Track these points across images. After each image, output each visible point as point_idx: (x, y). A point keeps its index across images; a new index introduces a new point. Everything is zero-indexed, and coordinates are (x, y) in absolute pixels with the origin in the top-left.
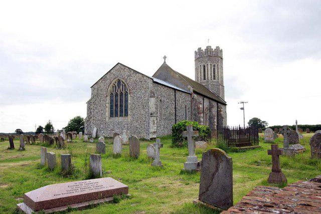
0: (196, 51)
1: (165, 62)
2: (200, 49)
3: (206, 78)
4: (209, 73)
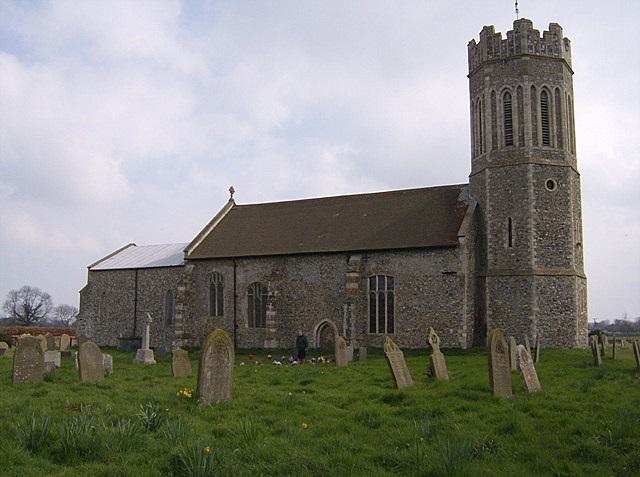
0: (472, 44)
2: (488, 32)
3: (516, 138)
4: (528, 111)
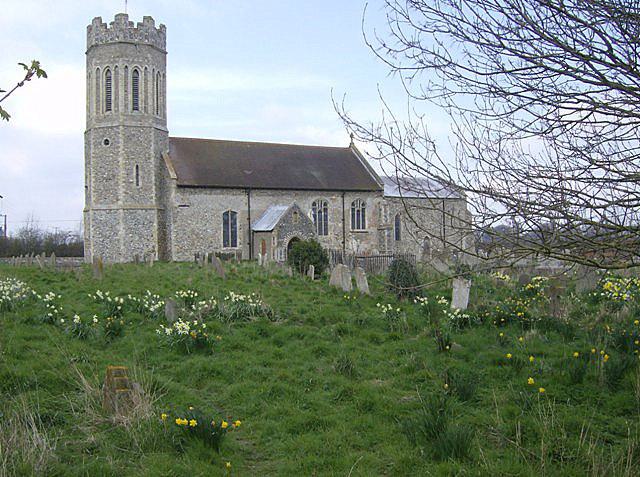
1: (352, 143)
